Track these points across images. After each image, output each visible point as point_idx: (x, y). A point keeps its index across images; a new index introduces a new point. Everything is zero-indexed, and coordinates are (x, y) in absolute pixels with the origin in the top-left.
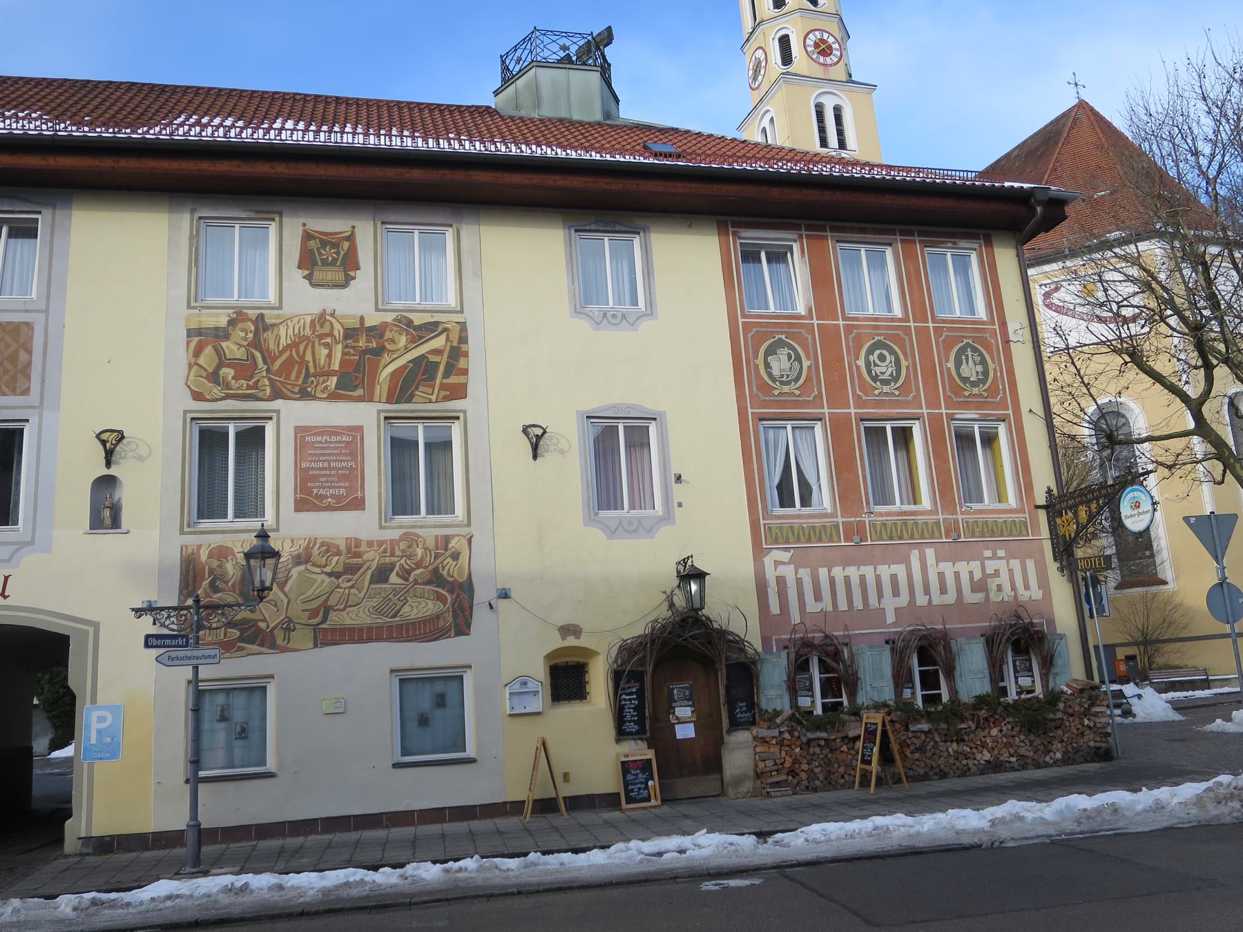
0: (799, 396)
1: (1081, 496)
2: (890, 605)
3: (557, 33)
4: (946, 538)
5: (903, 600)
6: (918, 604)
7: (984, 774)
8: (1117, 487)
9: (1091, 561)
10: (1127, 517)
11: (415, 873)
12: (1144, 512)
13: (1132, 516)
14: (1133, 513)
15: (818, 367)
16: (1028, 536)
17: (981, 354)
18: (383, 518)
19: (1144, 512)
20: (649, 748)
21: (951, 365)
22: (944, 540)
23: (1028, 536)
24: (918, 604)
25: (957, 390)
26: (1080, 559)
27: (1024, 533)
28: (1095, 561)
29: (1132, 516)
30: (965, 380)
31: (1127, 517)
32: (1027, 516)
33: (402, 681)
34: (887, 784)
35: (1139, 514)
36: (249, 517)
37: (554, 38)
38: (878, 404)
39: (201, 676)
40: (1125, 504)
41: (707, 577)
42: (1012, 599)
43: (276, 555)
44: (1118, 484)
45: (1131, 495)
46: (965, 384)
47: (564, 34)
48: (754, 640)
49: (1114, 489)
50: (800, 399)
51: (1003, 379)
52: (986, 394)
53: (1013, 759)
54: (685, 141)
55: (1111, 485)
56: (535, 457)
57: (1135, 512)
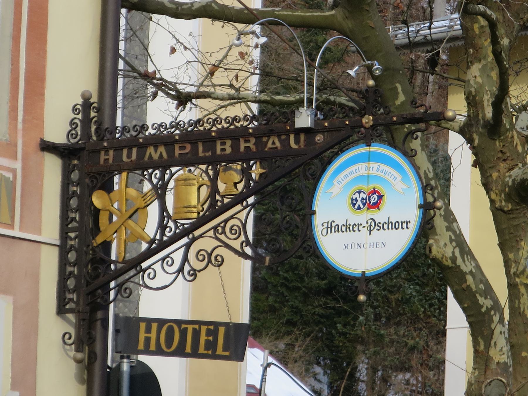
1: (194, 143)
4: (21, 230)
8: (319, 138)
10: (330, 227)
12: (391, 225)
13: (348, 227)
14: (355, 218)
16: (11, 226)
18: (239, 381)
19: (391, 225)
22: (16, 233)
23: (11, 226)
26: (149, 321)
27: (6, 219)
29: (348, 227)
31: (330, 227)
32: (18, 165)
36: (286, 368)
39: (431, 33)
40: (336, 189)
44: (324, 131)
45: (361, 168)
49: (310, 142)
55: (299, 131)
57: (355, 218)
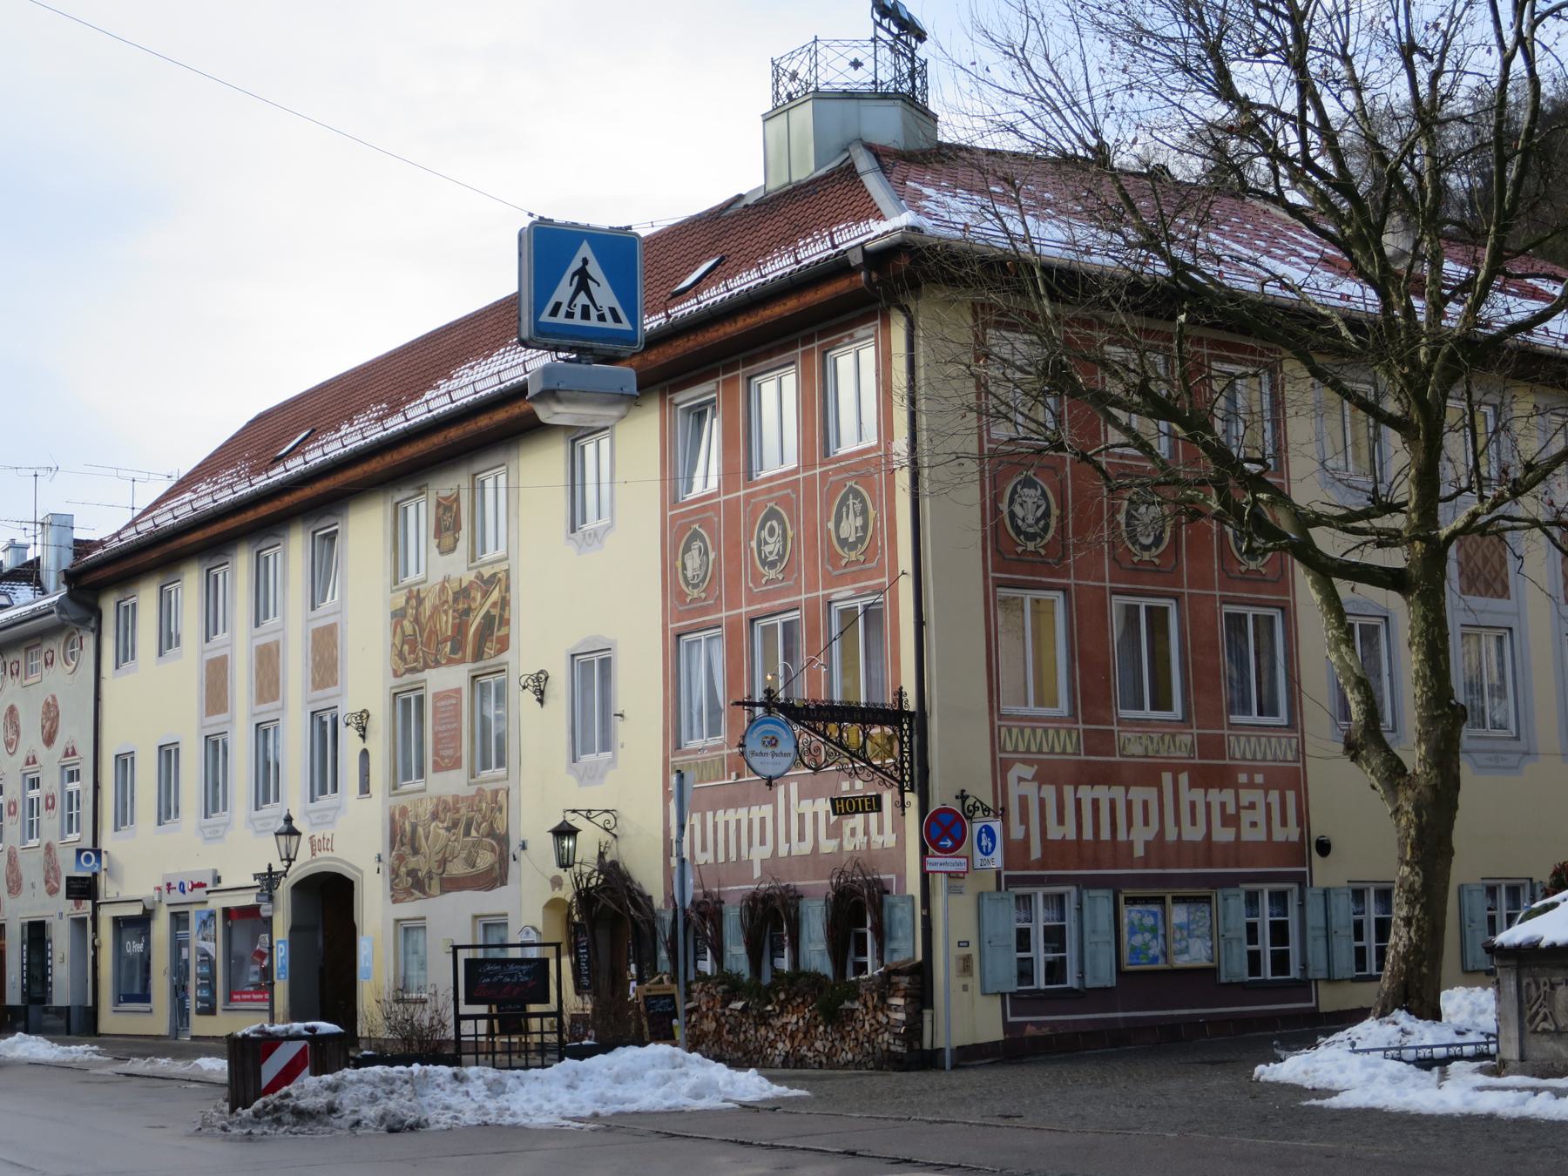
0: (705, 600)
2: (760, 853)
3: (846, 43)
5: (766, 851)
6: (780, 854)
7: (881, 1069)
9: (857, 803)
11: (619, 1091)
14: (764, 750)
15: (882, 517)
17: (863, 501)
20: (1485, 989)
21: (831, 525)
24: (780, 854)
25: (834, 558)
28: (863, 802)
30: (843, 542)
33: (486, 926)
34: (944, 1069)
35: (774, 754)
37: (842, 50)
38: (766, 596)
40: (755, 735)
41: (579, 834)
42: (864, 847)
43: (299, 834)
46: (843, 549)
47: (856, 44)
48: (659, 901)
50: (867, 566)
51: (882, 532)
52: (703, 595)
53: (810, 1054)
54: (657, 277)
56: (541, 701)
57: (770, 750)
